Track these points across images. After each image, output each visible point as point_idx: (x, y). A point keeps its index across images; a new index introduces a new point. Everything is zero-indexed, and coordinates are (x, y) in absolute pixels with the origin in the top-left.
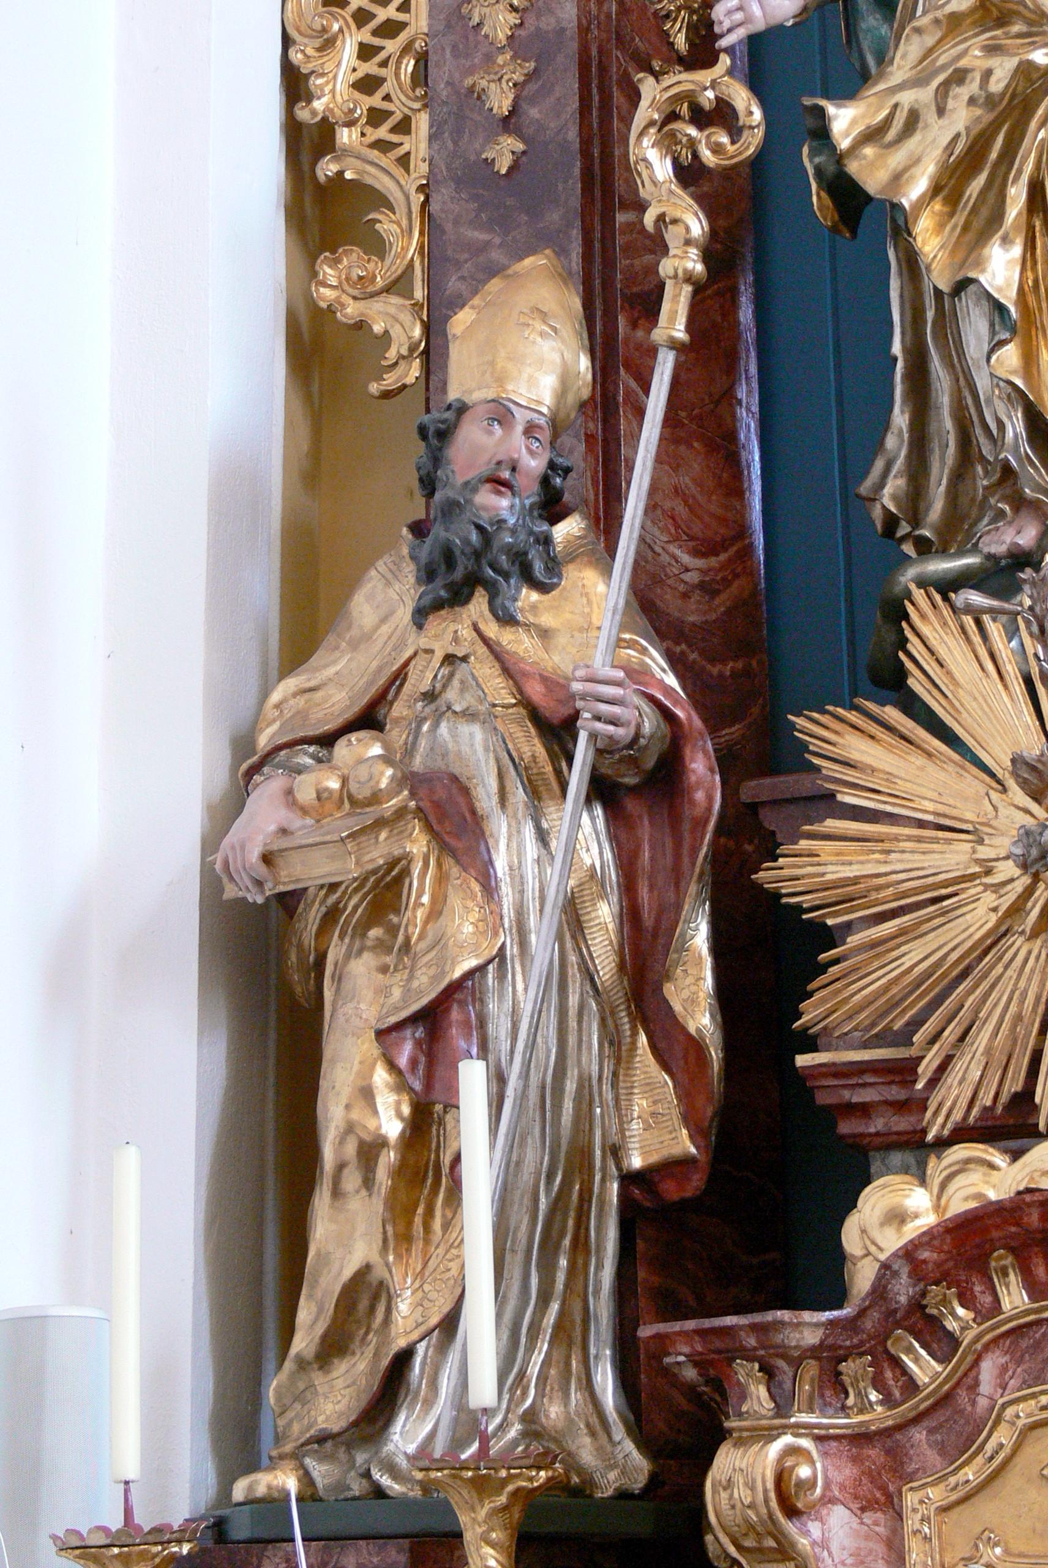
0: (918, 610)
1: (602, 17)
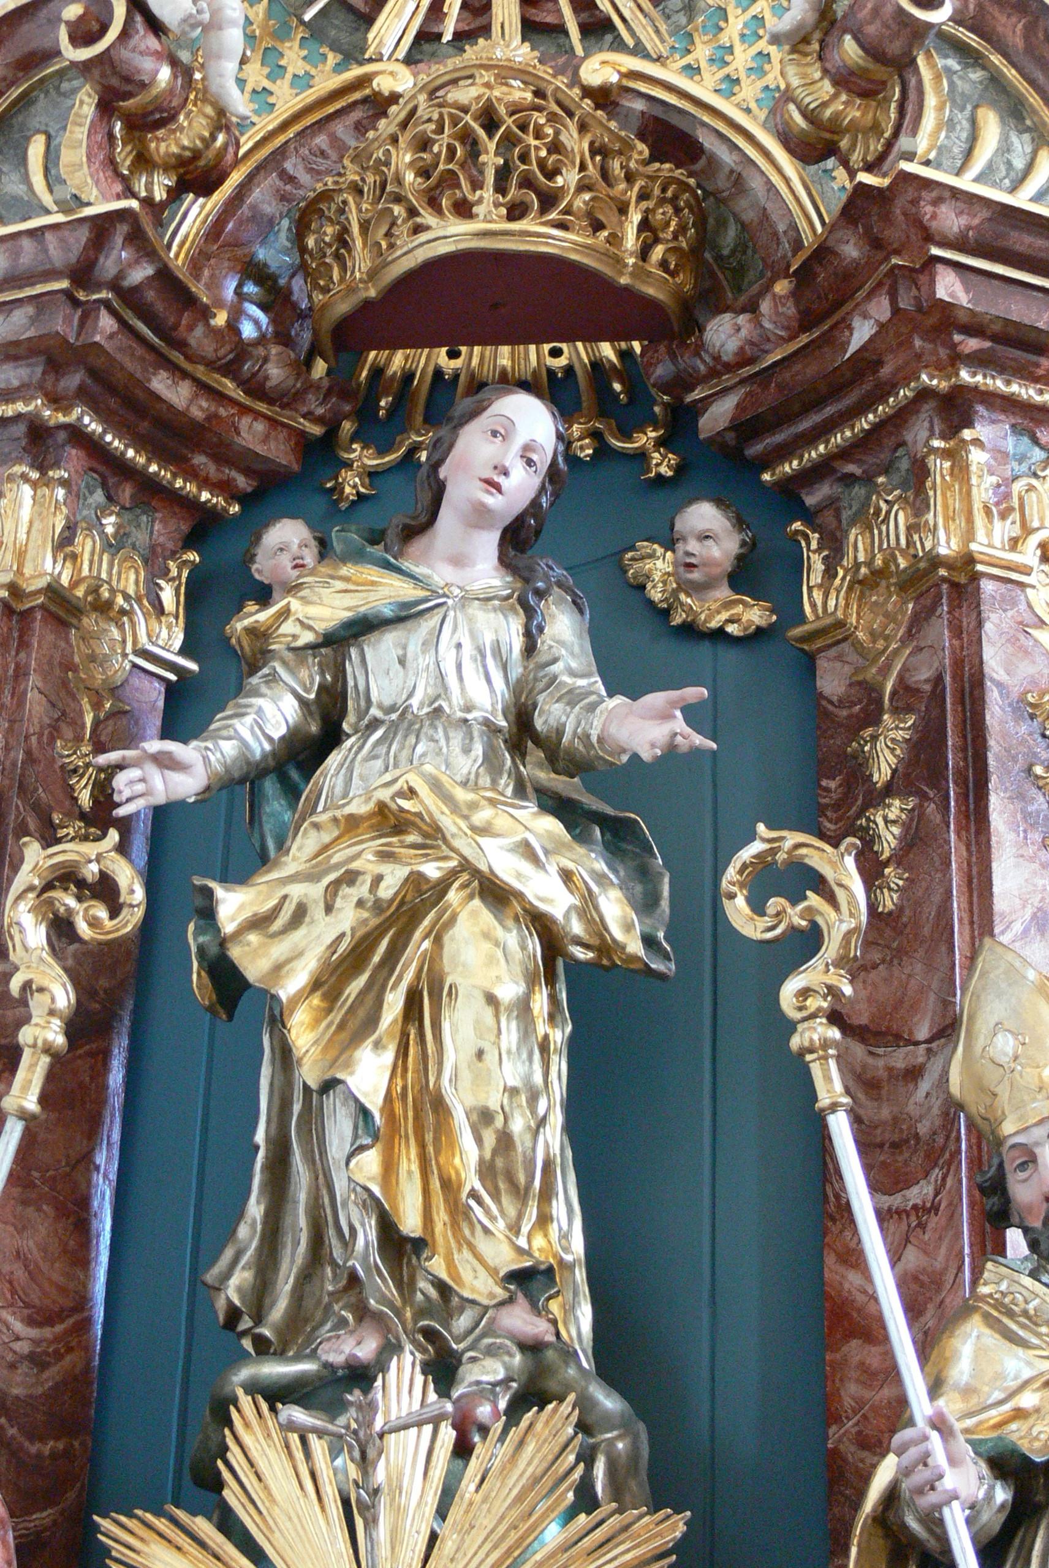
0: (242, 1417)
1: (8, 763)
